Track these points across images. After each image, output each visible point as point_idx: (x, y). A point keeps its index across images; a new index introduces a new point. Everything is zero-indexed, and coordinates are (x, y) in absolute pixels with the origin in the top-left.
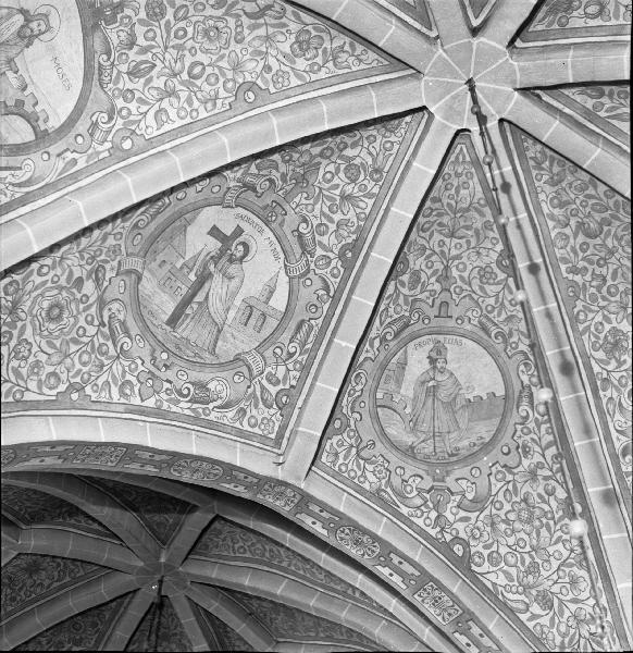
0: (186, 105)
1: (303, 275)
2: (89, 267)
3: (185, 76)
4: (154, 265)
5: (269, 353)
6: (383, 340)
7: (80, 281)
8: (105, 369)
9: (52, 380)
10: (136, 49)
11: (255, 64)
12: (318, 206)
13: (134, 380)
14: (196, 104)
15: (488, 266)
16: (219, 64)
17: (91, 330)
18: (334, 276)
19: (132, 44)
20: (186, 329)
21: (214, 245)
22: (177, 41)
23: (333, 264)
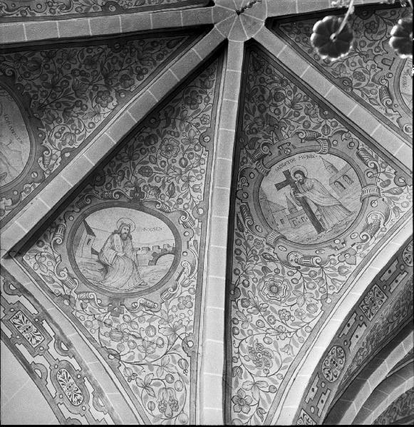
0: (196, 174)
1: (330, 144)
2: (260, 261)
3: (183, 170)
4: (280, 226)
5: (369, 181)
6: (390, 107)
7: (265, 269)
8: (324, 277)
9: (312, 308)
10: (161, 189)
11: (192, 131)
12: (292, 122)
13: (341, 264)
14: (198, 169)
15: (365, 26)
16: (185, 149)
17: (298, 275)
18: (336, 125)
20: (328, 223)
21: (288, 190)
23: (329, 124)
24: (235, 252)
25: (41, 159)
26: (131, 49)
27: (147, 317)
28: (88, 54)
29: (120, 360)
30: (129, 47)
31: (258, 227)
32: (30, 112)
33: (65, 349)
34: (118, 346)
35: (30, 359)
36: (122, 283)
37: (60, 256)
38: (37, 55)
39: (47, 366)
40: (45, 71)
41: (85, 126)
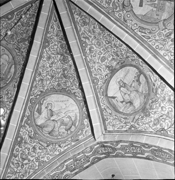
0: (114, 41)
2: (167, 40)
3: (110, 44)
4: (159, 17)
10: (114, 57)
11: (96, 31)
14: (112, 39)
16: (102, 38)
19: (114, 59)
22: (106, 50)
24: (156, 48)
25: (77, 97)
26: (50, 38)
27: (158, 105)
28: (45, 58)
29: (165, 130)
30: (49, 39)
31: (153, 29)
32: (59, 90)
33: (147, 146)
34: (160, 125)
35: (144, 156)
36: (140, 101)
37: (115, 115)
38: (37, 79)
39: (150, 154)
40: (45, 78)
41: (73, 73)
